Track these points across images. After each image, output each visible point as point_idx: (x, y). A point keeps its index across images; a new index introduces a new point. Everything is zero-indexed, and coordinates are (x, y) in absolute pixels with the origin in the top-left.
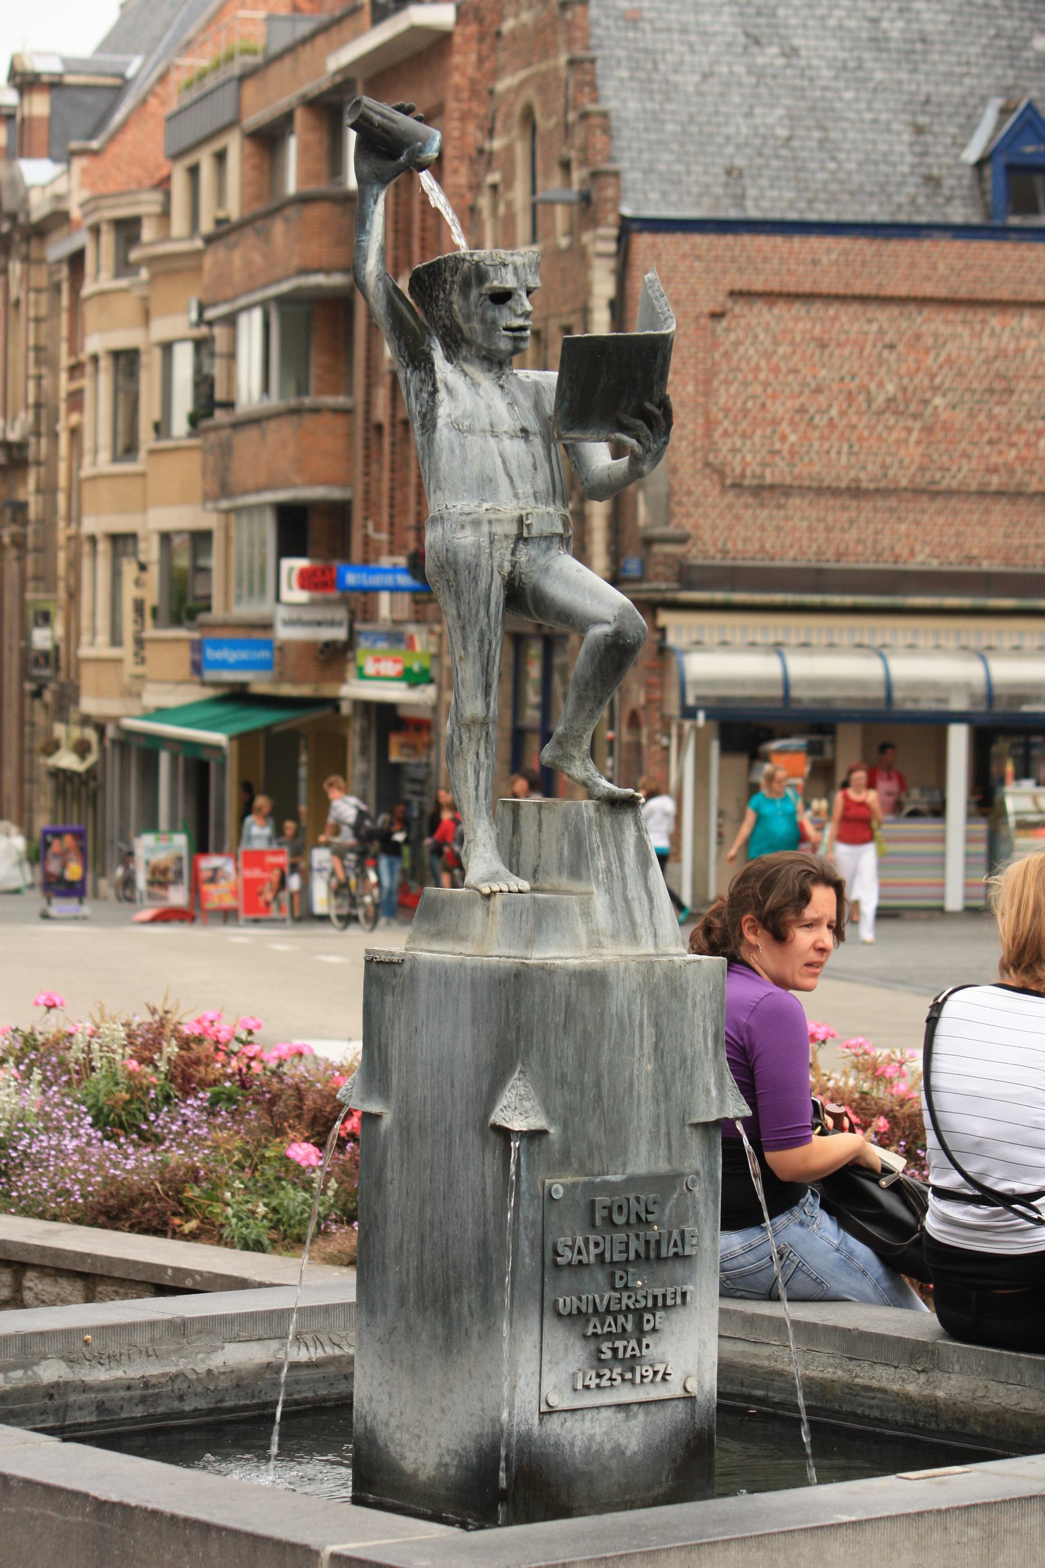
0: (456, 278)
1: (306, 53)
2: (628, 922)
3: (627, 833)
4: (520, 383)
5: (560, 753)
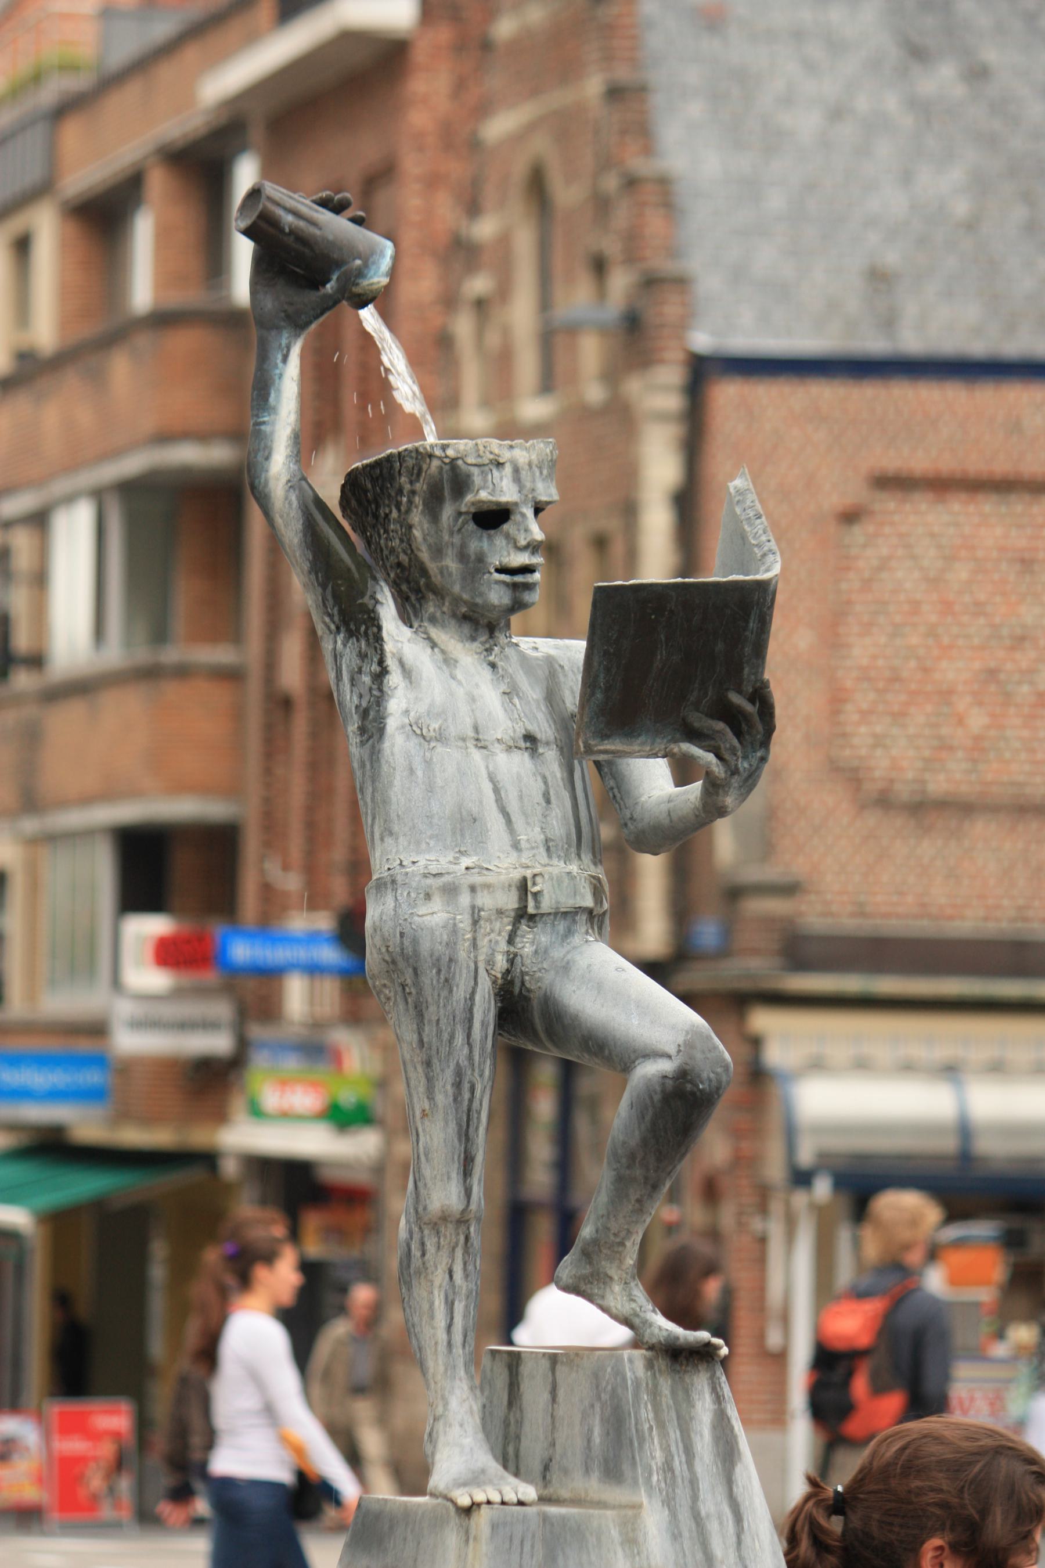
0: (418, 486)
1: (166, 73)
2: (700, 1556)
3: (699, 1405)
4: (523, 658)
5: (587, 1270)
